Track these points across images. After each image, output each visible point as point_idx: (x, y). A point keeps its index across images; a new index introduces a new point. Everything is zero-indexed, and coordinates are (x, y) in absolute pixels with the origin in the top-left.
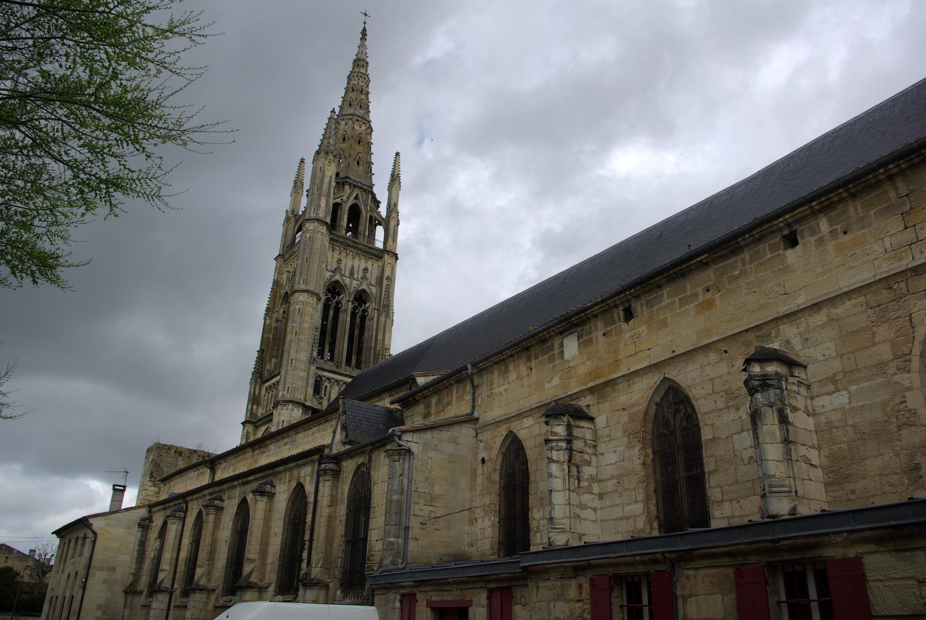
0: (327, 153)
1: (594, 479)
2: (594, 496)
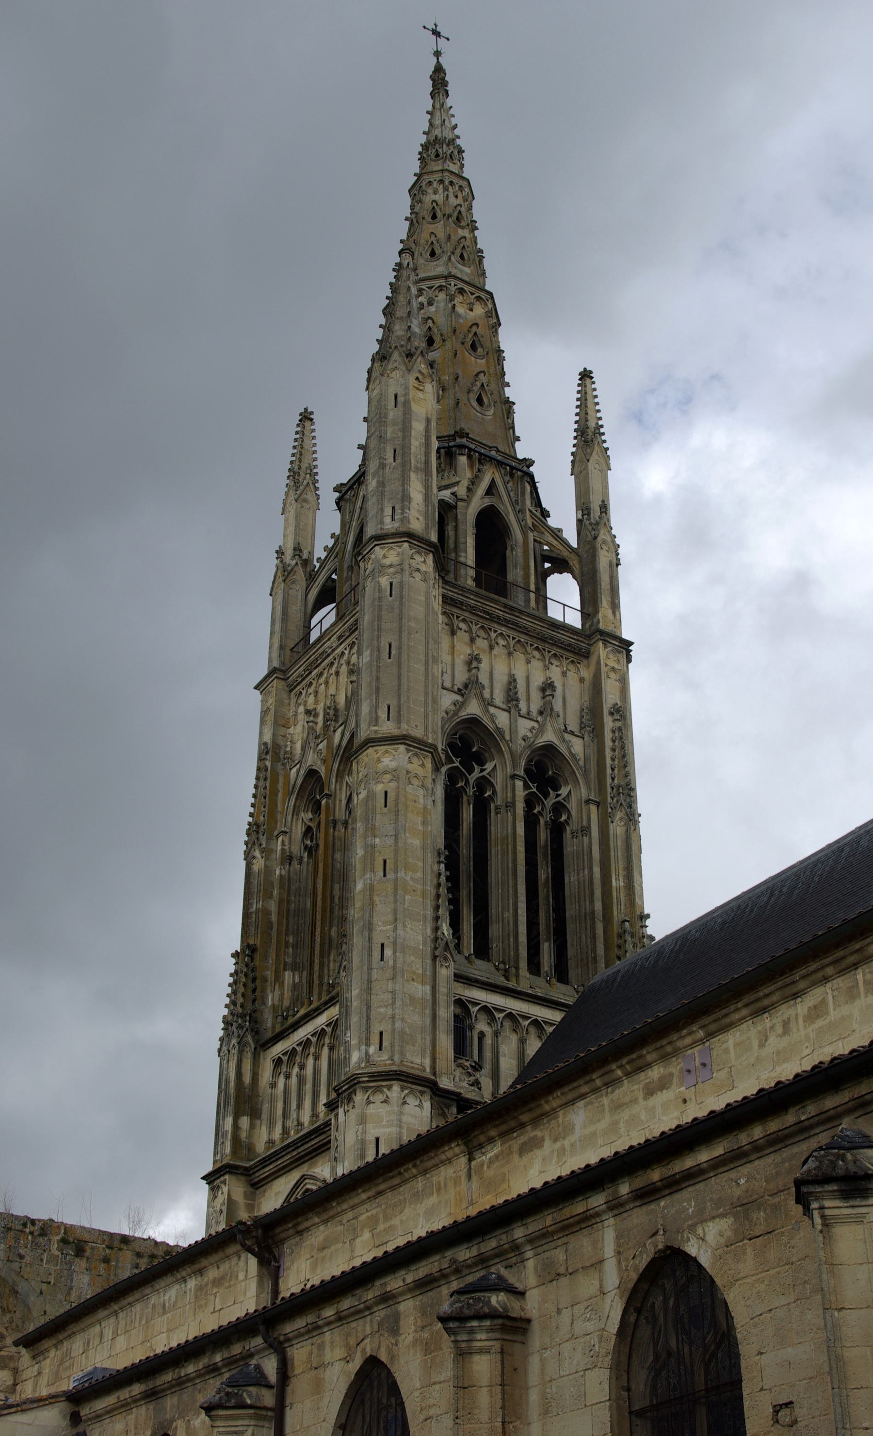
0: (409, 355)
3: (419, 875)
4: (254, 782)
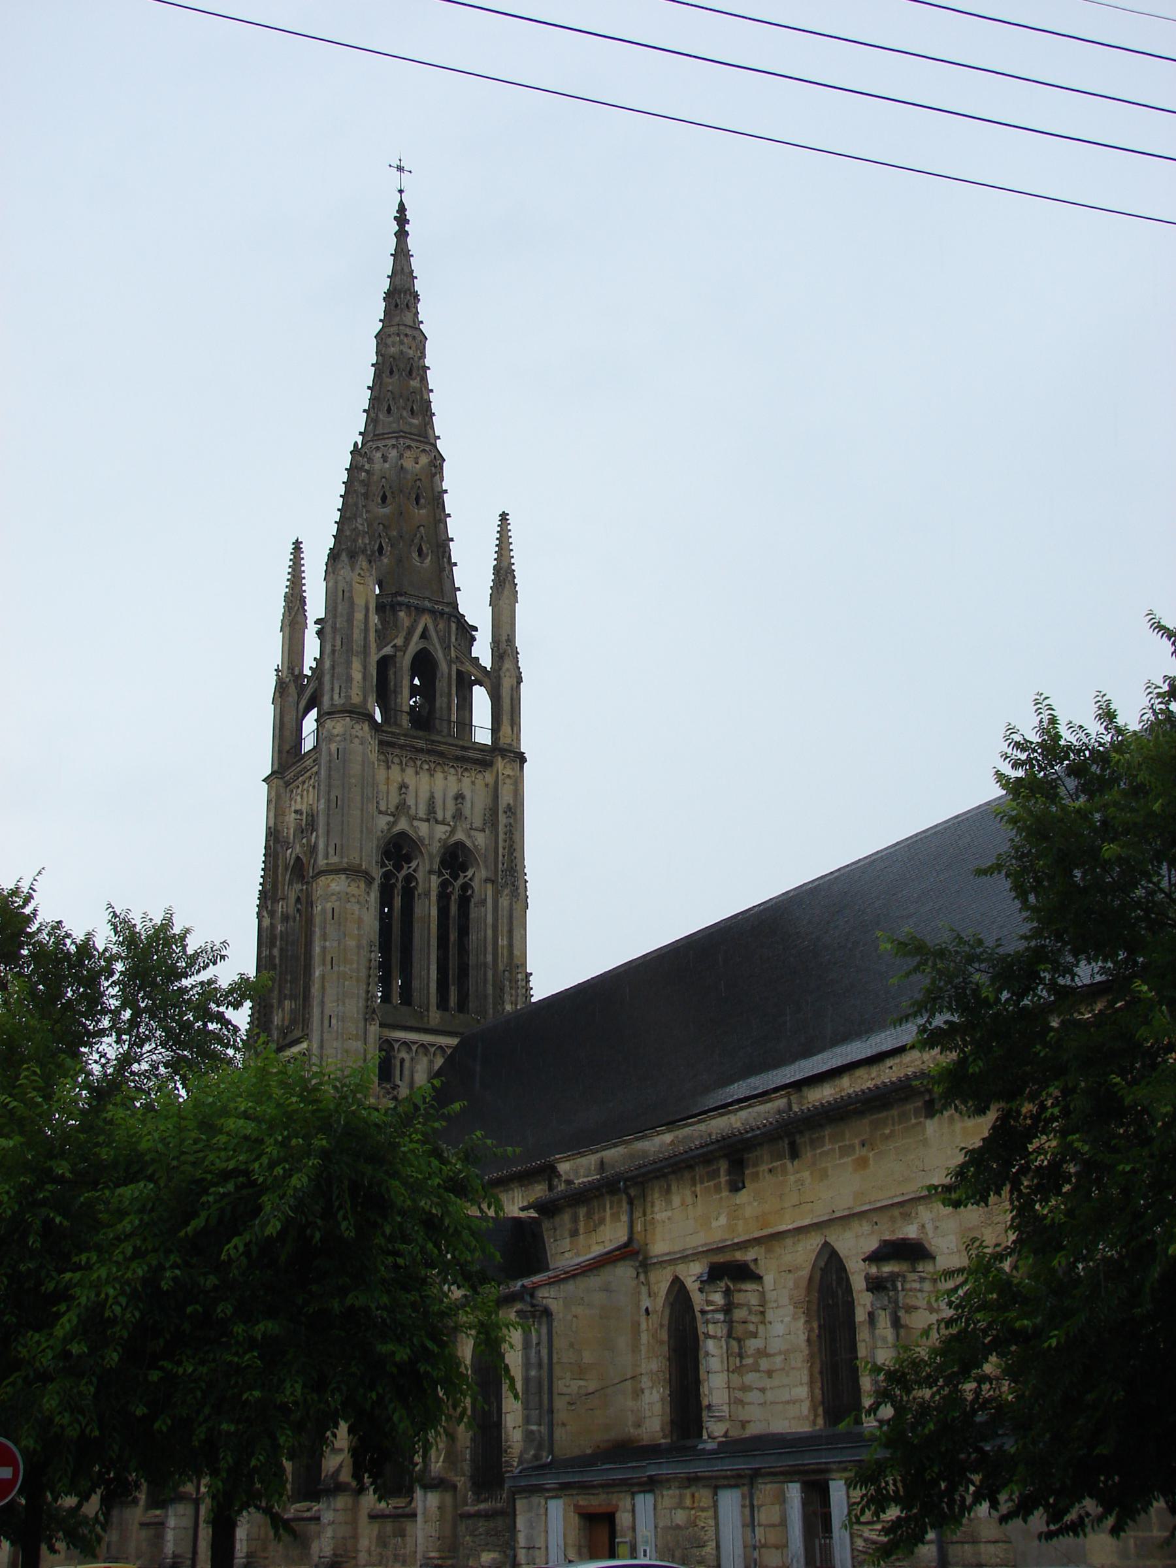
1: (762, 1353)
2: (763, 1374)
3: (355, 966)
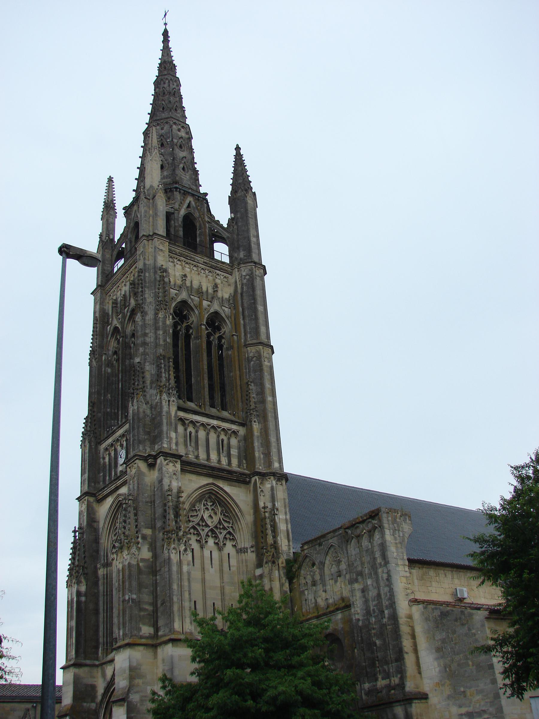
4: (92, 333)
